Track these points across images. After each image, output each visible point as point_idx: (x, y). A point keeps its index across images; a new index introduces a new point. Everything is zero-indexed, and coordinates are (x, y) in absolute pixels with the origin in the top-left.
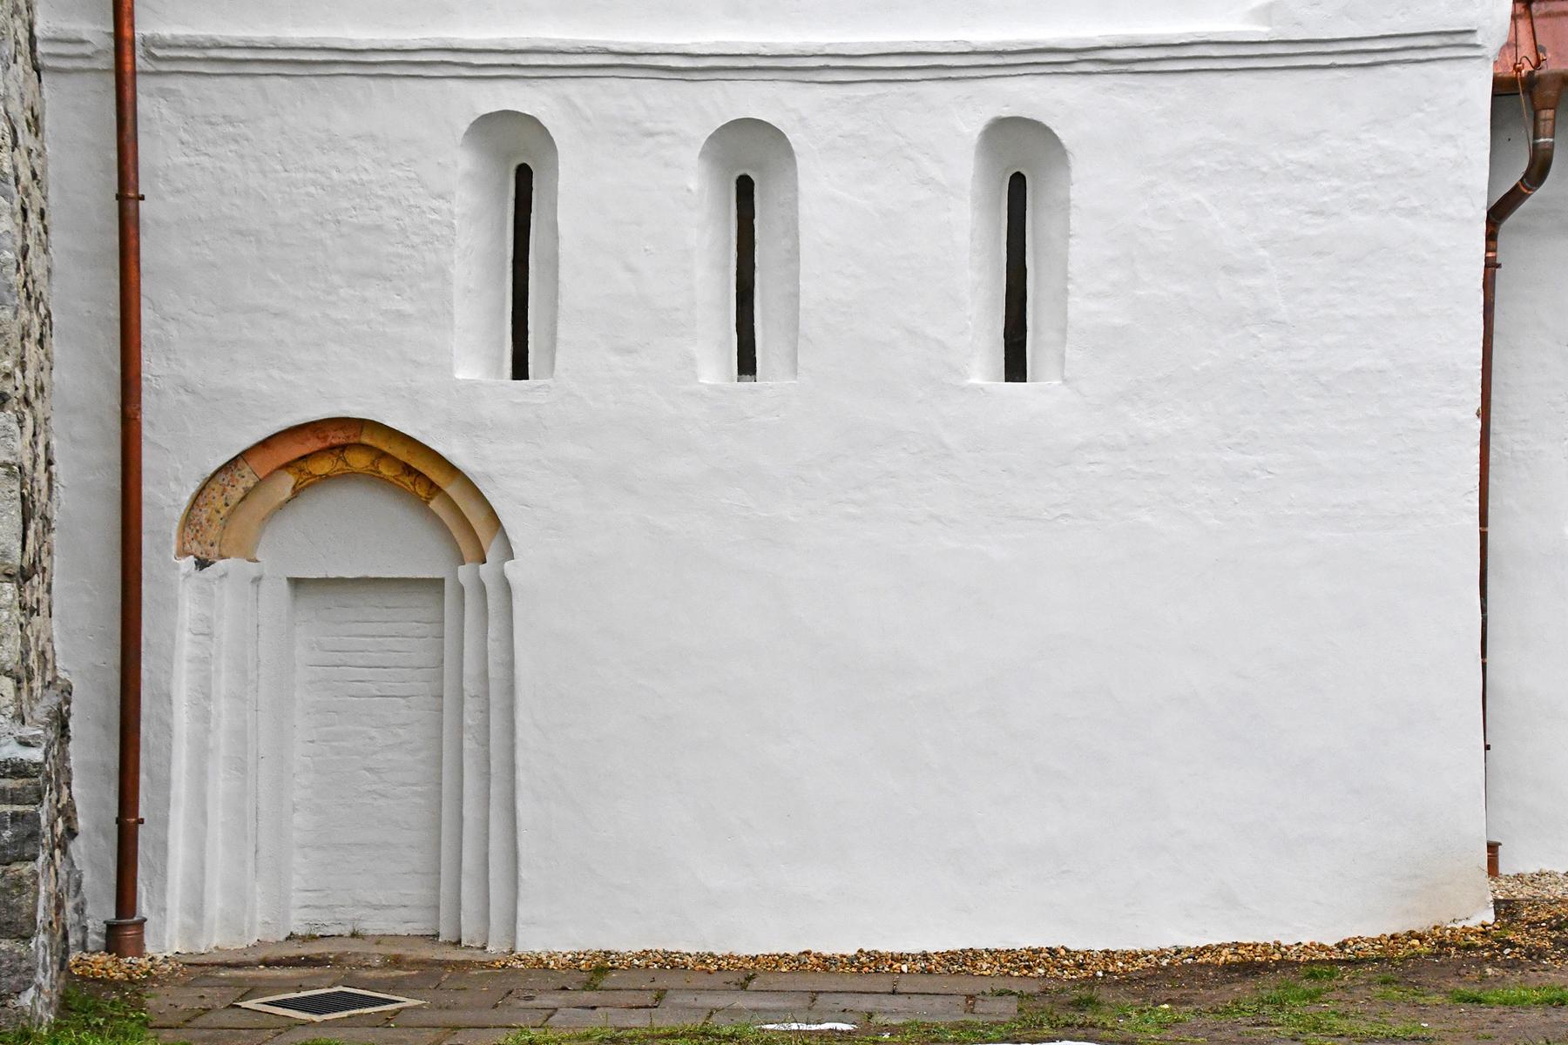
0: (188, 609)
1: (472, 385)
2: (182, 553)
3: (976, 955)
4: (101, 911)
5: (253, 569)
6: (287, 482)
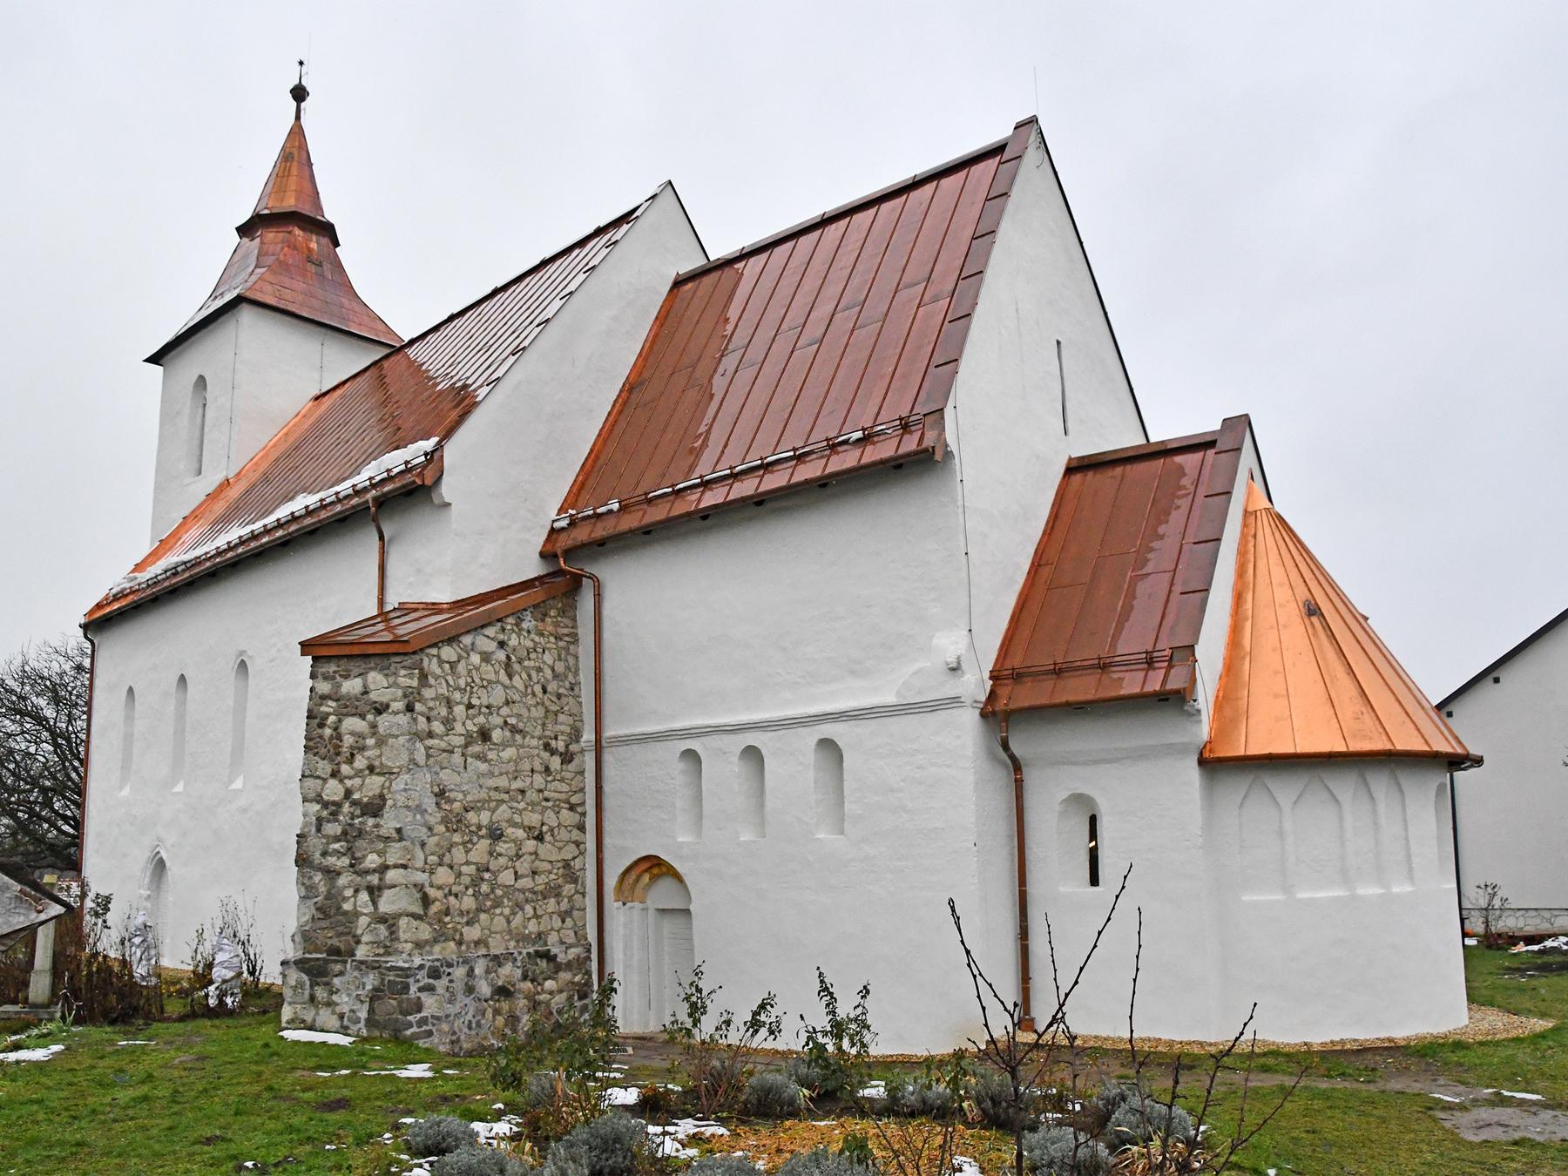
2: (617, 901)
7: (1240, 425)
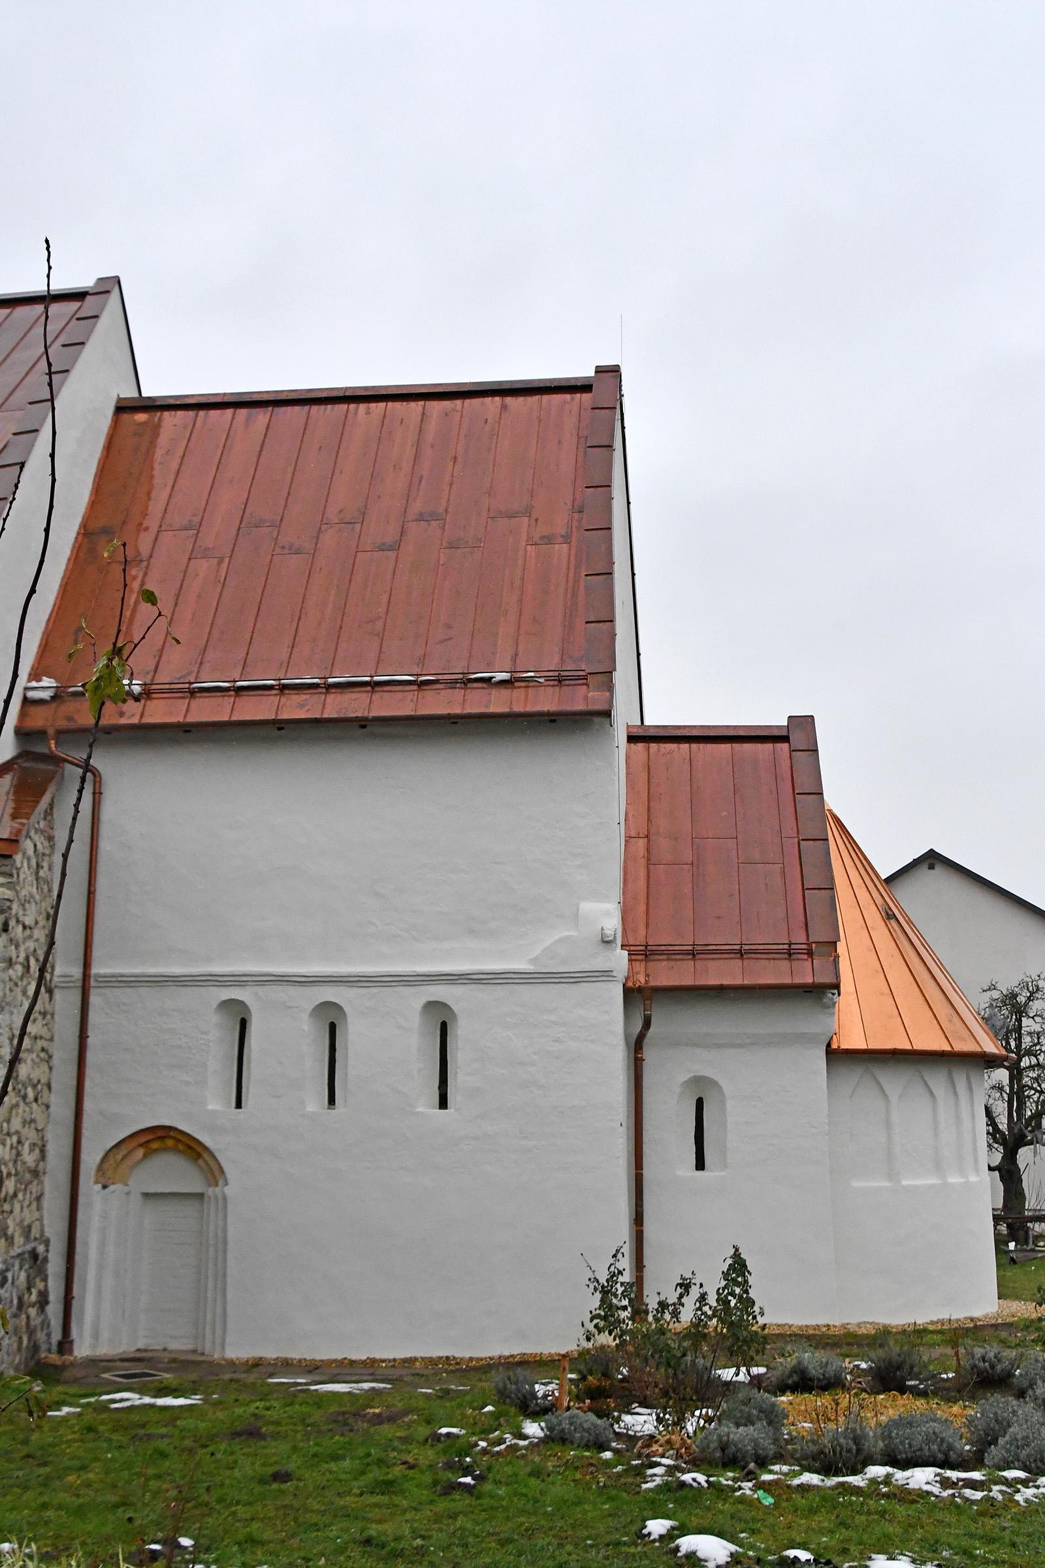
0: (98, 1206)
1: (214, 1112)
2: (96, 1182)
3: (416, 1359)
4: (56, 1336)
5: (126, 1189)
6: (140, 1153)
7: (110, 286)
